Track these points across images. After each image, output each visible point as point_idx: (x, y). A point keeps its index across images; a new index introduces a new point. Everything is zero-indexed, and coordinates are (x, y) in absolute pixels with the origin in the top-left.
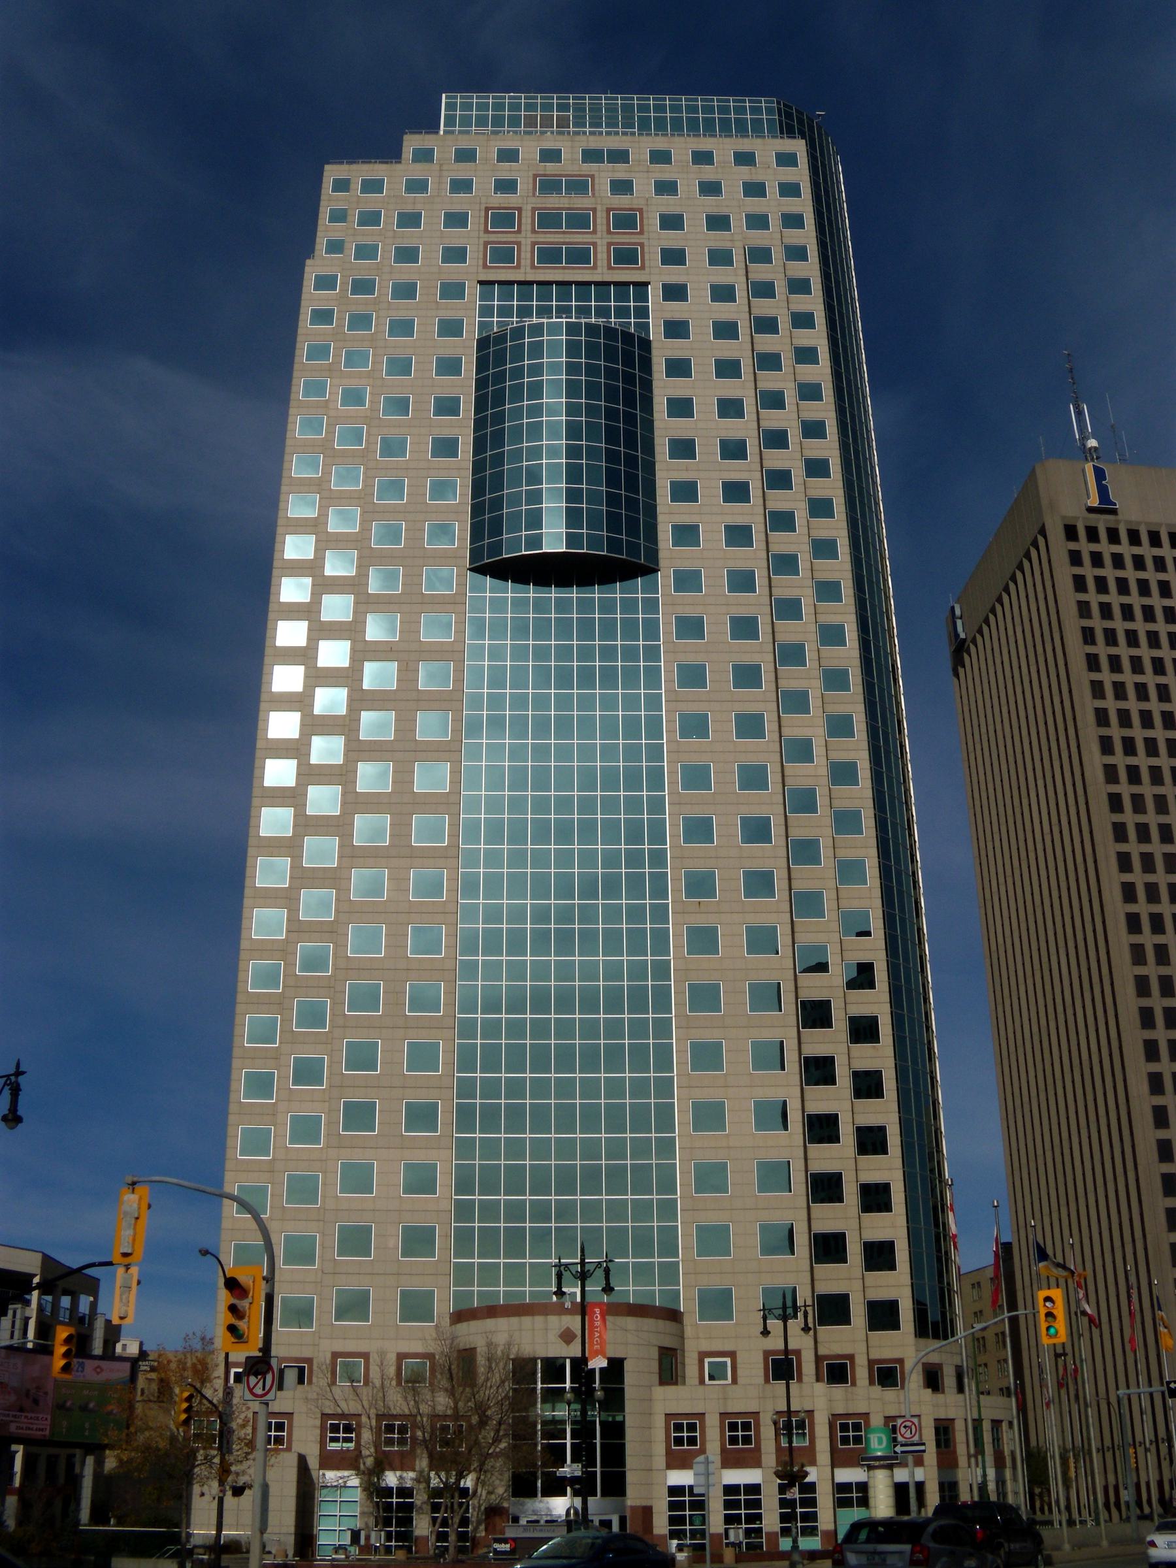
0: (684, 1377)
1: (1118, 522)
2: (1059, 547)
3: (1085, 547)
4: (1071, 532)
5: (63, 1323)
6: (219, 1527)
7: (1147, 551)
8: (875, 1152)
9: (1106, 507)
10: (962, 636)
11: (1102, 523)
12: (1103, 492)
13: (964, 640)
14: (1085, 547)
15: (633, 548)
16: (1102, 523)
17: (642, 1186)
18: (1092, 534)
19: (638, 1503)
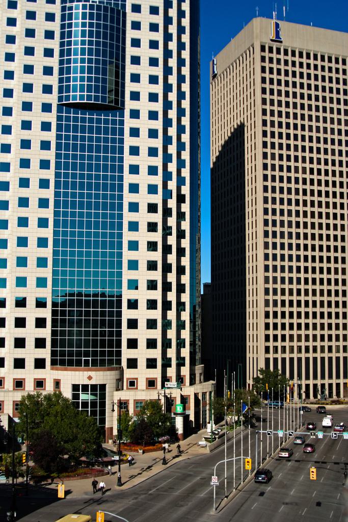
0: (44, 298)
1: (281, 46)
2: (258, 54)
3: (267, 54)
4: (263, 49)
5: (120, 457)
6: (120, 467)
7: (289, 58)
8: (153, 270)
9: (278, 39)
10: (216, 72)
11: (275, 46)
12: (277, 33)
13: (216, 74)
14: (267, 54)
15: (117, 102)
16: (275, 46)
17: (111, 346)
18: (271, 50)
19: (109, 427)
